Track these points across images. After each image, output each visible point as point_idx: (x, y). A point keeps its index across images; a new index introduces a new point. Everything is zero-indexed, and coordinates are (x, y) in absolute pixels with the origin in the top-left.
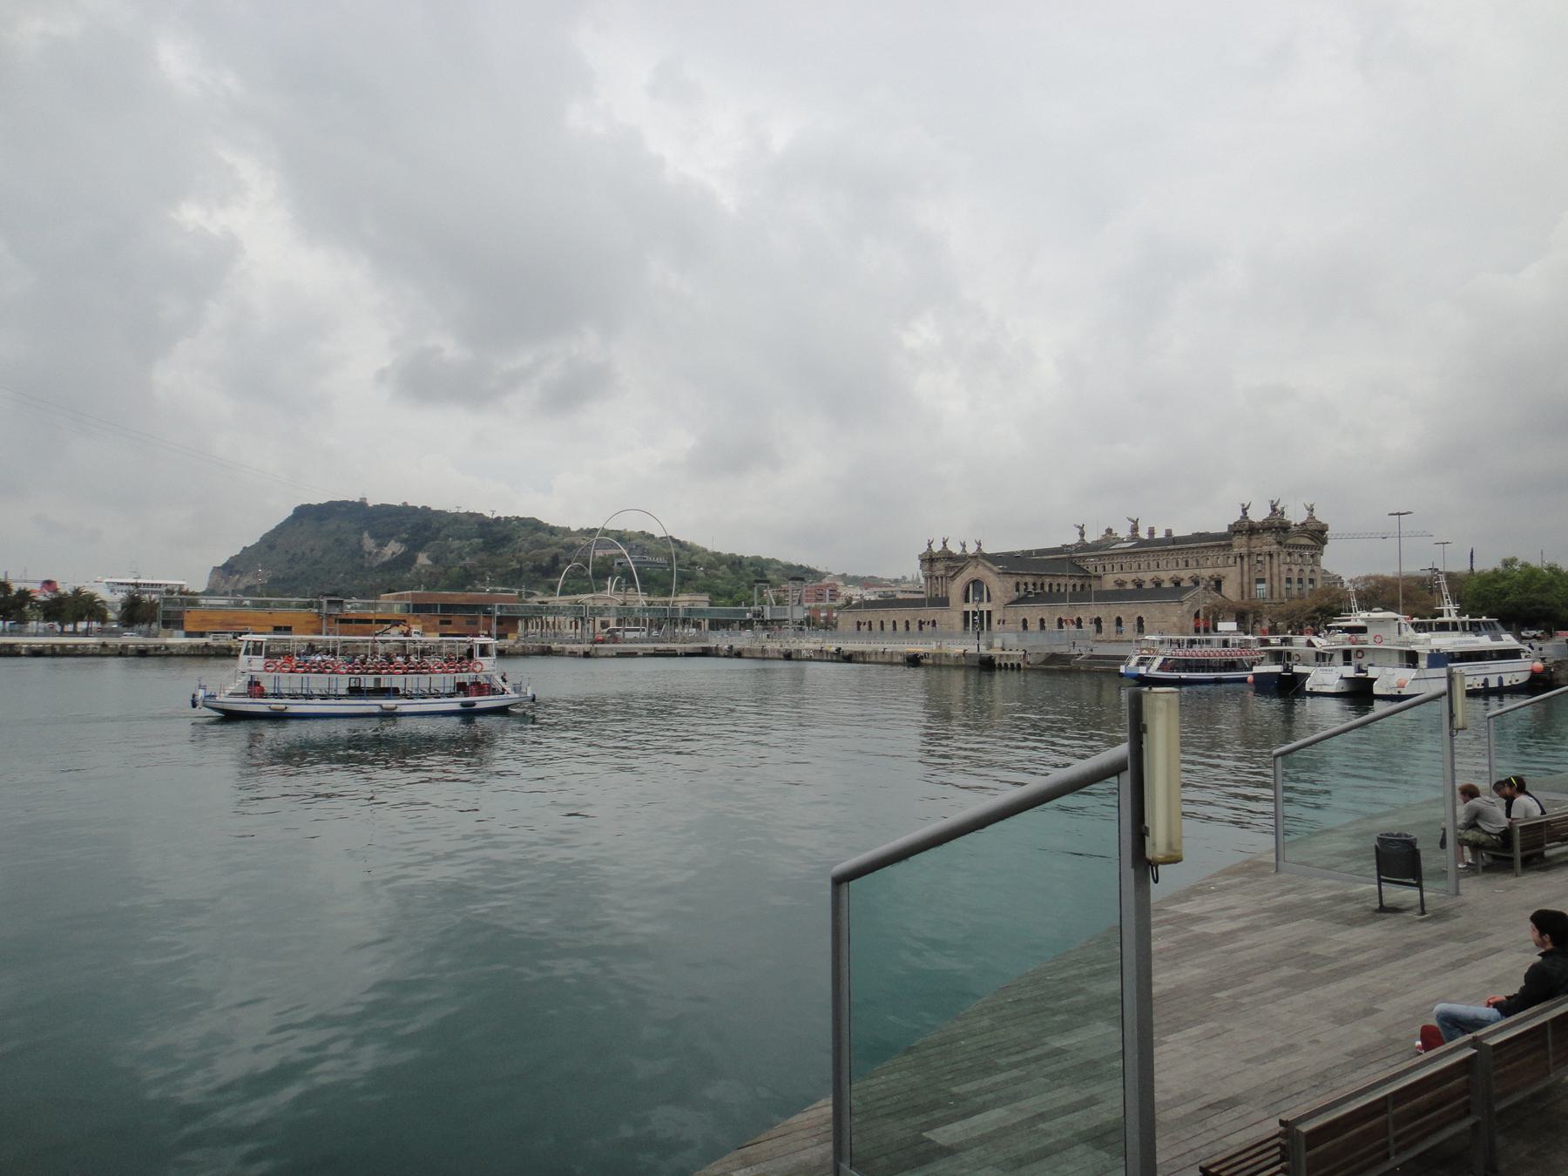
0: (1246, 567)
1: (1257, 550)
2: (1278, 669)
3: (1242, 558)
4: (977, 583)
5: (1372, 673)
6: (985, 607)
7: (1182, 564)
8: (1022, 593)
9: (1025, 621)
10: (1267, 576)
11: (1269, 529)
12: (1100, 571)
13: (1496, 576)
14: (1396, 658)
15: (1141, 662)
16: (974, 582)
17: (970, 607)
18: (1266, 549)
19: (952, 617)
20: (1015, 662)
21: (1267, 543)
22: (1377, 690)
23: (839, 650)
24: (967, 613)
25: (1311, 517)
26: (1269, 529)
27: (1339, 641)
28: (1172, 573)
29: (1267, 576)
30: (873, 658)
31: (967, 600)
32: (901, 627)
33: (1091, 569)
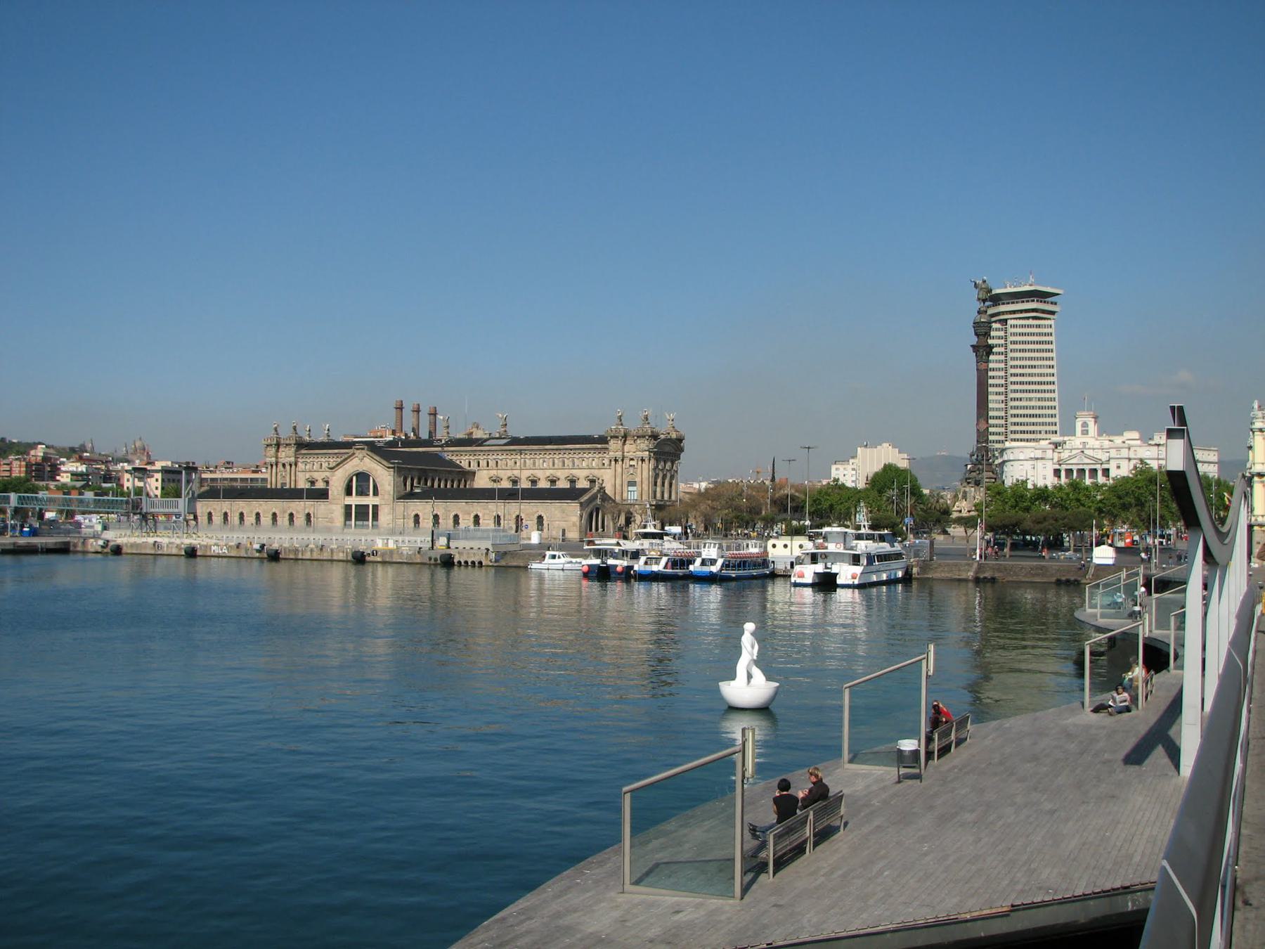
0: (619, 470)
1: (630, 455)
2: (597, 562)
3: (616, 461)
4: (363, 477)
5: (835, 569)
6: (370, 500)
7: (558, 463)
9: (417, 516)
12: (474, 467)
14: (847, 559)
16: (359, 475)
17: (354, 500)
19: (330, 511)
20: (476, 559)
22: (839, 581)
28: (548, 473)
29: (638, 480)
30: (308, 556)
32: (217, 519)
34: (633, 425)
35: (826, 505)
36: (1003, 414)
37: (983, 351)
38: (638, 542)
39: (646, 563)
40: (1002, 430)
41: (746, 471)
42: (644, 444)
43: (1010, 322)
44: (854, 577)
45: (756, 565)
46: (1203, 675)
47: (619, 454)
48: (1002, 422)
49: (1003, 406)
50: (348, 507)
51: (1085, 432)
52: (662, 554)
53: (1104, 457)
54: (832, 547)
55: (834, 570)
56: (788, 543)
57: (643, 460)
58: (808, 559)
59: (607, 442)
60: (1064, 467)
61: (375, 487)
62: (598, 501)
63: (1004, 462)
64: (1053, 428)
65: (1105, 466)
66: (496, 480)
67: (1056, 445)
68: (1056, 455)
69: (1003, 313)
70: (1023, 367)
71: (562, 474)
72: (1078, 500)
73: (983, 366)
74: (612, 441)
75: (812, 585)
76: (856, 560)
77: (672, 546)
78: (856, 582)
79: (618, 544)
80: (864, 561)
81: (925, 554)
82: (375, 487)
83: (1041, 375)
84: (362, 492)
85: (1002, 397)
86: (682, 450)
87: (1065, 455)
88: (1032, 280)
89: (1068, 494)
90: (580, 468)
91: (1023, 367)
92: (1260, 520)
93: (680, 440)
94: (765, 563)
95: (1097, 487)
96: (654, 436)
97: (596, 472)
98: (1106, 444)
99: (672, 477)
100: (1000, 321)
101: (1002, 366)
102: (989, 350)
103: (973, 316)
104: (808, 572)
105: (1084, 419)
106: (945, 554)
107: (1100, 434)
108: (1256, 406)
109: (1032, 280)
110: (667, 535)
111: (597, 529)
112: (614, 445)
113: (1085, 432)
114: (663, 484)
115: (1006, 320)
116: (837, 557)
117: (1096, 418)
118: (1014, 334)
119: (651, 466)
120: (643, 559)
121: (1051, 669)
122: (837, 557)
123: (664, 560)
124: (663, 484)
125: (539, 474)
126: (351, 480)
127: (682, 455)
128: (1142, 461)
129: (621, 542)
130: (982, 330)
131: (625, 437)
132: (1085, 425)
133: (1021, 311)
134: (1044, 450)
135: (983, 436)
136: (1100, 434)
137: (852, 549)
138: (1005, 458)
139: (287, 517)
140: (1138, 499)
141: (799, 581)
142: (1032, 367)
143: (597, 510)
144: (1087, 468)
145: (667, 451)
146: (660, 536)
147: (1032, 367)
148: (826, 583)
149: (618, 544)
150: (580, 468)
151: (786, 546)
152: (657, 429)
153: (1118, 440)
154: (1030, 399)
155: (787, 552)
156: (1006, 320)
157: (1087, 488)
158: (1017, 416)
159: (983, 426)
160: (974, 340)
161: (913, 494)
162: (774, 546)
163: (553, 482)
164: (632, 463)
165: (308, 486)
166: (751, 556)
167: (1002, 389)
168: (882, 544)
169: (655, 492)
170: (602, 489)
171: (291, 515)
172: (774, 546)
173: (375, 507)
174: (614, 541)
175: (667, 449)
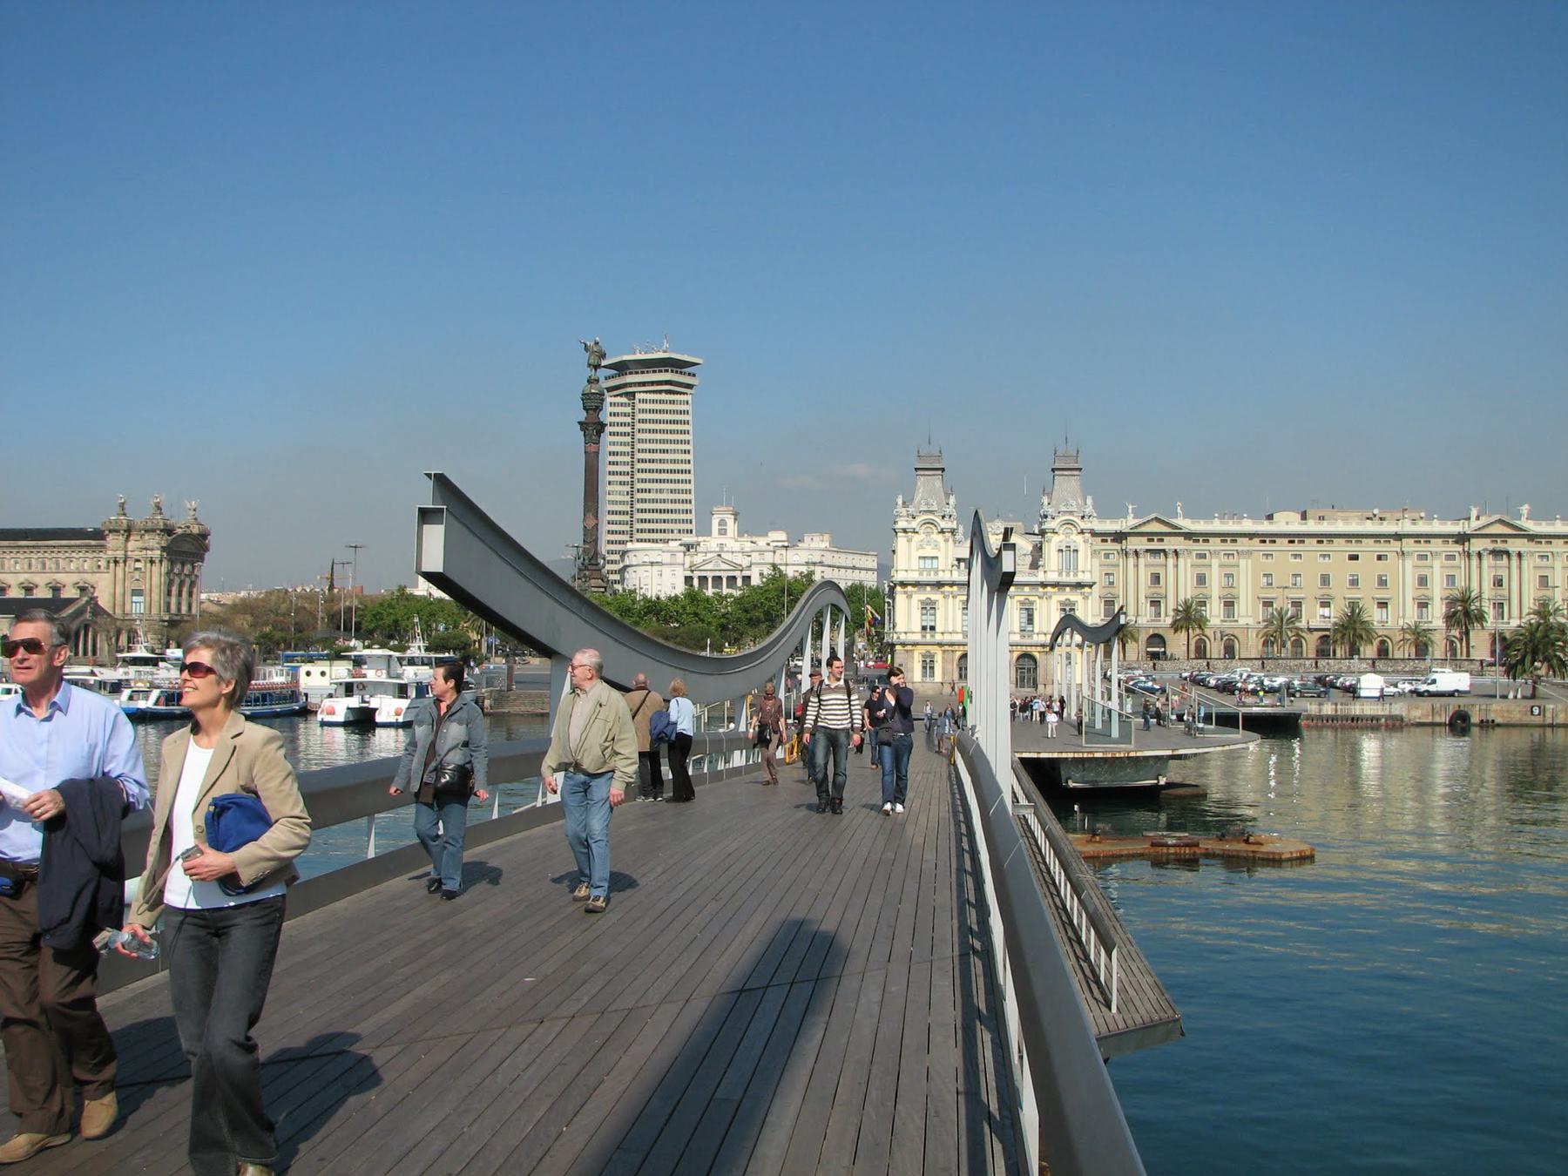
1: (137, 554)
3: (116, 562)
7: (36, 565)
22: (379, 718)
28: (22, 578)
34: (140, 516)
35: (388, 621)
36: (627, 508)
37: (593, 428)
38: (121, 670)
39: (131, 698)
40: (626, 528)
41: (303, 579)
42: (155, 542)
43: (638, 396)
44: (398, 714)
45: (282, 698)
47: (120, 554)
48: (627, 518)
49: (628, 498)
51: (723, 532)
52: (153, 686)
53: (745, 562)
54: (372, 675)
55: (373, 705)
56: (327, 670)
57: (152, 562)
58: (342, 690)
59: (103, 538)
60: (697, 574)
62: (88, 616)
63: (626, 567)
64: (688, 526)
65: (746, 573)
67: (689, 547)
68: (688, 559)
69: (630, 385)
70: (653, 451)
71: (41, 580)
72: (696, 614)
73: (593, 448)
74: (111, 537)
75: (345, 725)
76: (402, 691)
77: (167, 674)
78: (401, 719)
79: (93, 674)
80: (412, 693)
81: (501, 683)
83: (675, 461)
85: (628, 488)
86: (206, 549)
87: (698, 559)
88: (666, 345)
89: (684, 608)
90: (67, 572)
91: (653, 451)
92: (903, 637)
93: (204, 536)
94: (294, 695)
95: (721, 598)
96: (168, 531)
97: (90, 578)
98: (748, 546)
99: (193, 584)
100: (627, 394)
101: (628, 449)
102: (601, 427)
103: (582, 385)
104: (341, 707)
105: (722, 516)
106: (525, 682)
107: (740, 534)
108: (900, 502)
109: (666, 345)
110: (163, 660)
111: (85, 653)
112: (113, 541)
113: (723, 532)
114: (180, 594)
115: (633, 394)
116: (378, 688)
117: (736, 515)
118: (644, 411)
119: (164, 570)
120: (126, 693)
122: (378, 688)
123: (155, 693)
124: (180, 594)
125: (61, 577)
127: (207, 556)
128: (774, 566)
129: (96, 670)
130: (593, 403)
131: (128, 532)
132: (722, 522)
133: (652, 383)
134: (673, 554)
135: (591, 536)
136: (740, 534)
137: (399, 676)
138: (627, 562)
140: (767, 613)
141: (328, 718)
142: (664, 451)
143: (86, 627)
144: (724, 575)
145: (185, 550)
146: (153, 662)
147: (664, 451)
148: (363, 722)
149: (93, 674)
150: (67, 572)
151: (323, 674)
152: (172, 522)
153: (762, 542)
154: (661, 491)
155: (325, 681)
156: (633, 394)
157: (707, 600)
158: (645, 511)
159: (591, 522)
160: (583, 416)
162: (308, 674)
163: (29, 590)
164: (138, 565)
165: (49, 595)
166: (274, 687)
167: (628, 478)
169: (168, 605)
170: (93, 599)
172: (308, 674)
174: (87, 669)
175: (186, 547)
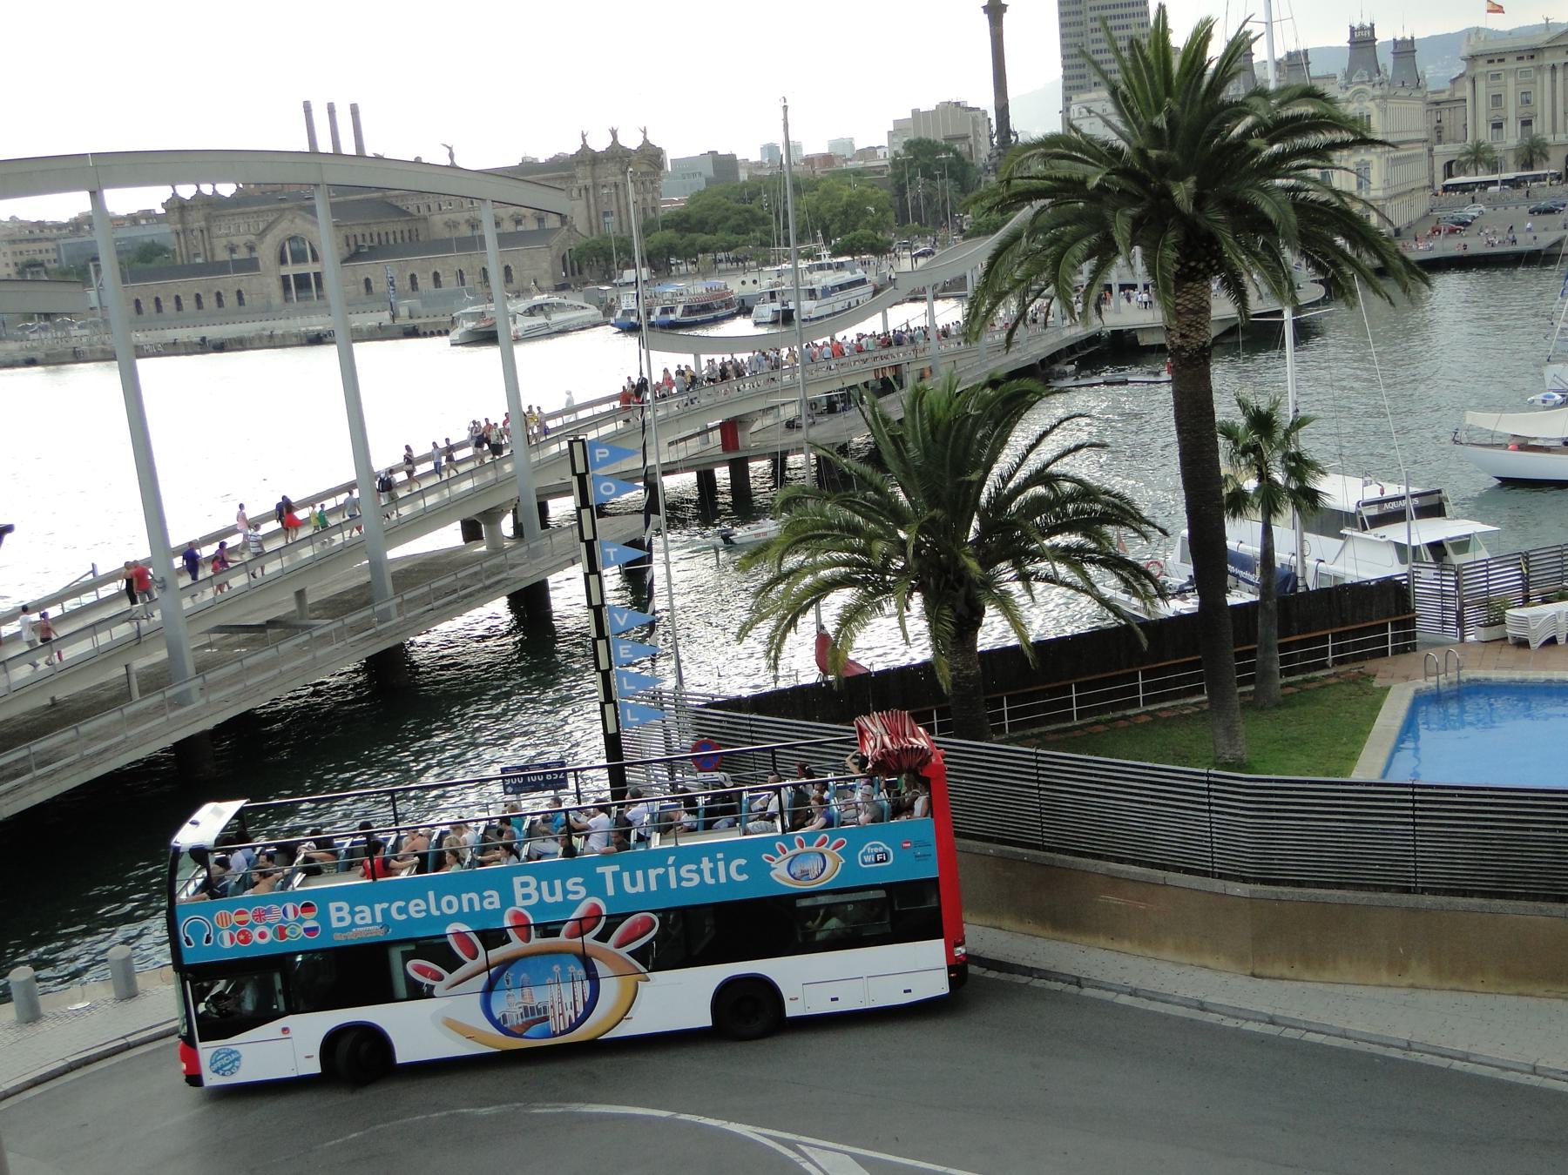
3: (586, 189)
6: (309, 268)
8: (353, 248)
10: (614, 208)
11: (613, 158)
13: (827, 159)
15: (665, 311)
16: (292, 239)
17: (291, 270)
18: (611, 179)
21: (610, 174)
23: (203, 339)
24: (285, 279)
25: (646, 141)
26: (613, 158)
27: (1365, 375)
31: (283, 261)
32: (189, 304)
33: (413, 210)
46: (785, 119)
50: (285, 279)
61: (313, 251)
66: (452, 225)
82: (313, 251)
84: (299, 257)
121: (1108, 592)
126: (283, 247)
139: (214, 298)
161: (977, 313)
168: (840, 274)
171: (219, 295)
173: (318, 276)
